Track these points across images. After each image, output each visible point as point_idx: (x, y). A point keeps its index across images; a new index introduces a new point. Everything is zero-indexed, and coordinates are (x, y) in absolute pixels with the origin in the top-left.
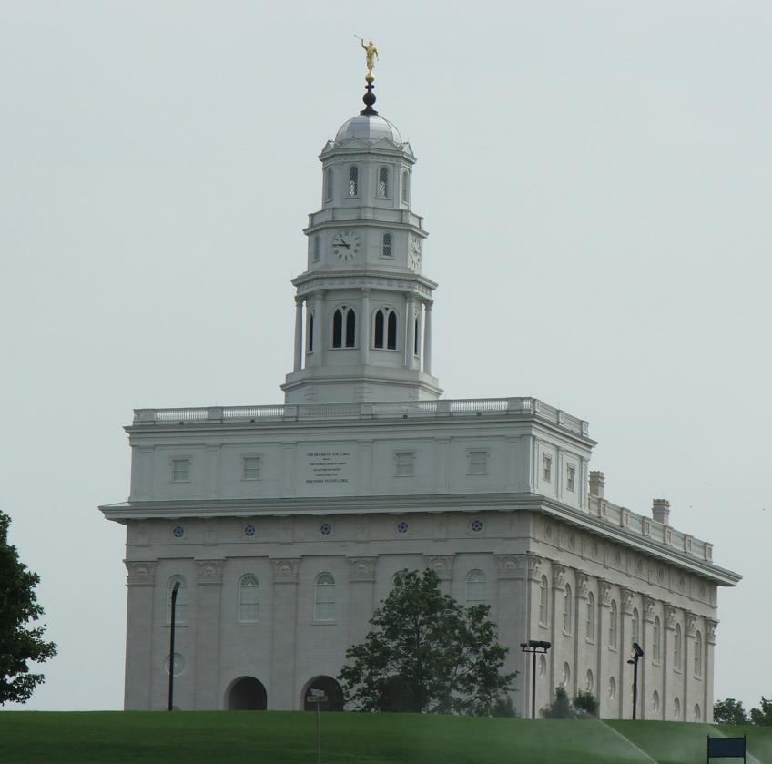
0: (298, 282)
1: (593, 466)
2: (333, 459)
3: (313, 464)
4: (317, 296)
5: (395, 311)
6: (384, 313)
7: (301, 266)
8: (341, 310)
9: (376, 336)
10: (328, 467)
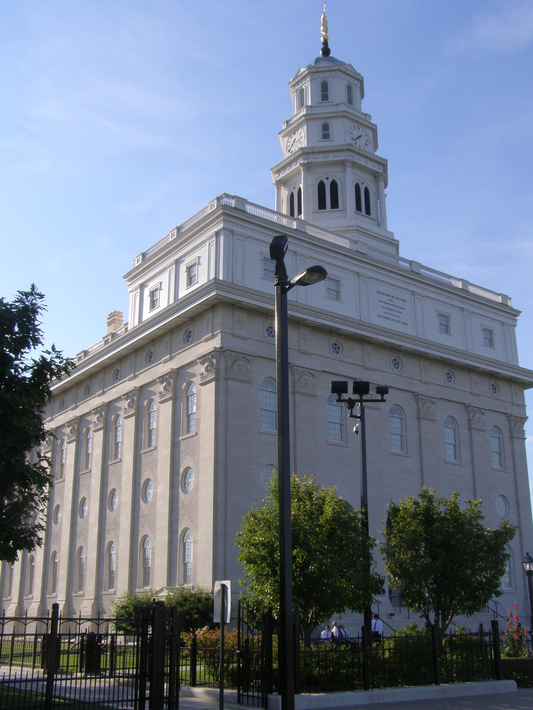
2: (396, 302)
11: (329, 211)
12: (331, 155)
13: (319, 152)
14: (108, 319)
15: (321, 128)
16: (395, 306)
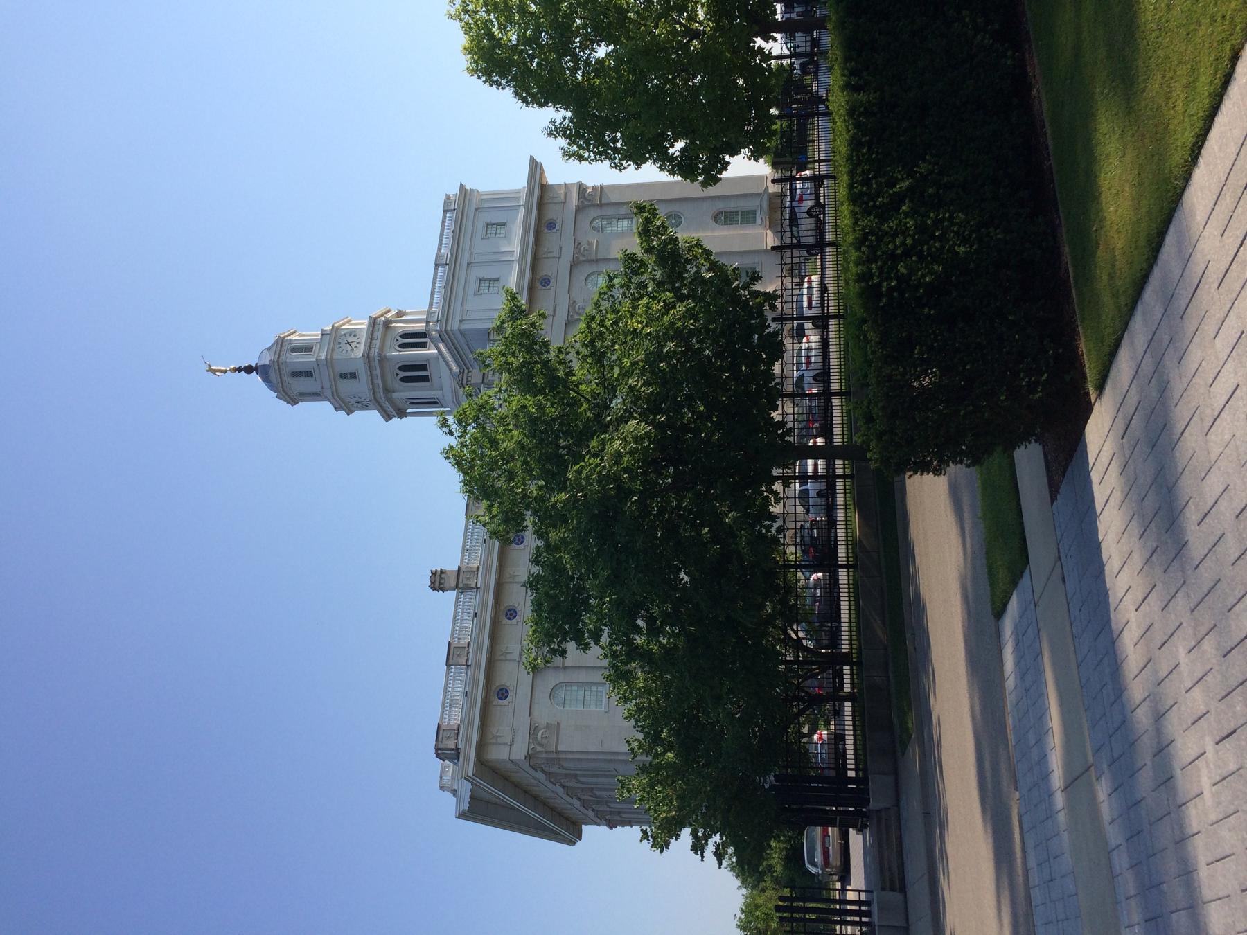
0: (388, 417)
1: (494, 86)
4: (390, 397)
6: (400, 343)
7: (374, 415)
8: (399, 377)
9: (418, 338)
12: (374, 373)
13: (371, 343)
15: (345, 380)
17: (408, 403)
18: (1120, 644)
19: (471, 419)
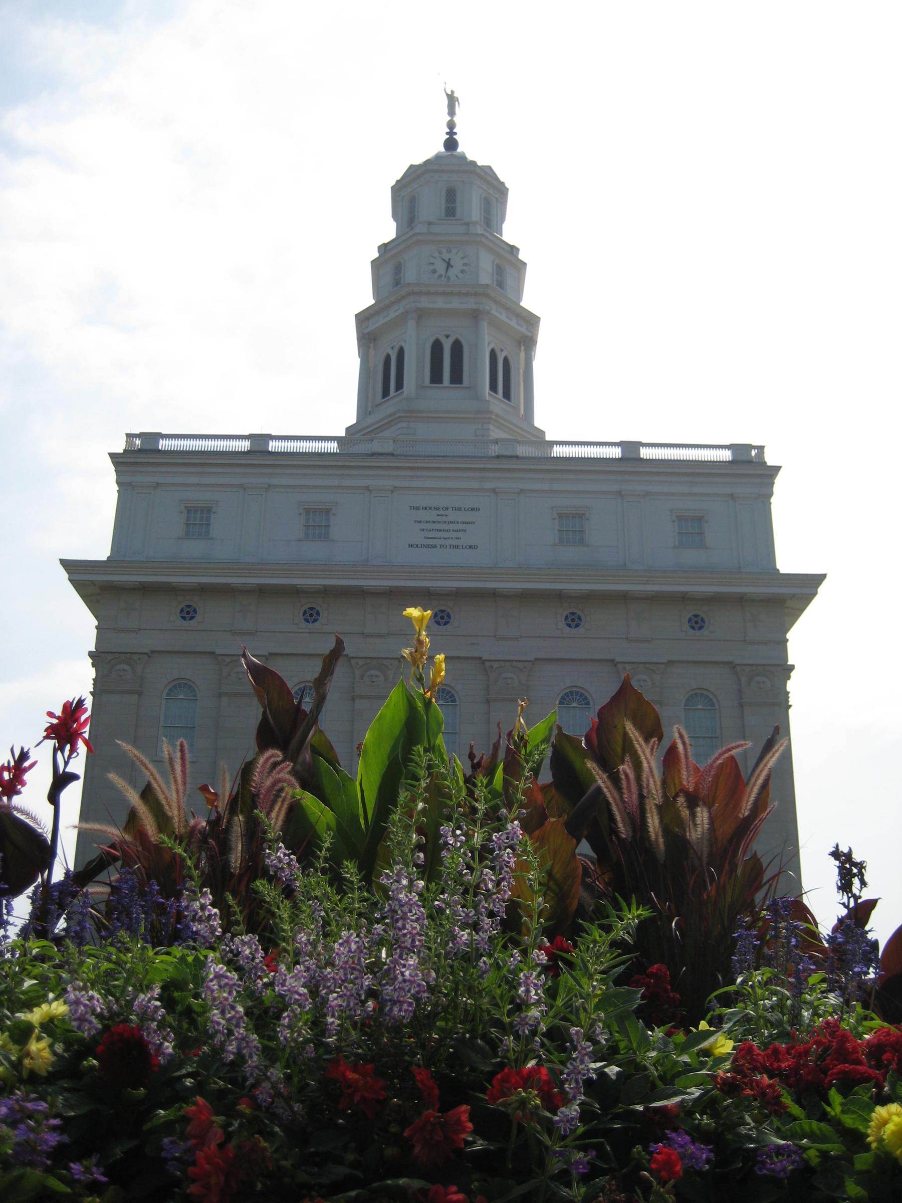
2: (453, 516)
3: (420, 522)
5: (461, 339)
8: (443, 340)
10: (445, 527)
11: (447, 387)
14: (871, 904)
16: (451, 522)
17: (391, 352)
18: (45, 1019)
19: (137, 894)
